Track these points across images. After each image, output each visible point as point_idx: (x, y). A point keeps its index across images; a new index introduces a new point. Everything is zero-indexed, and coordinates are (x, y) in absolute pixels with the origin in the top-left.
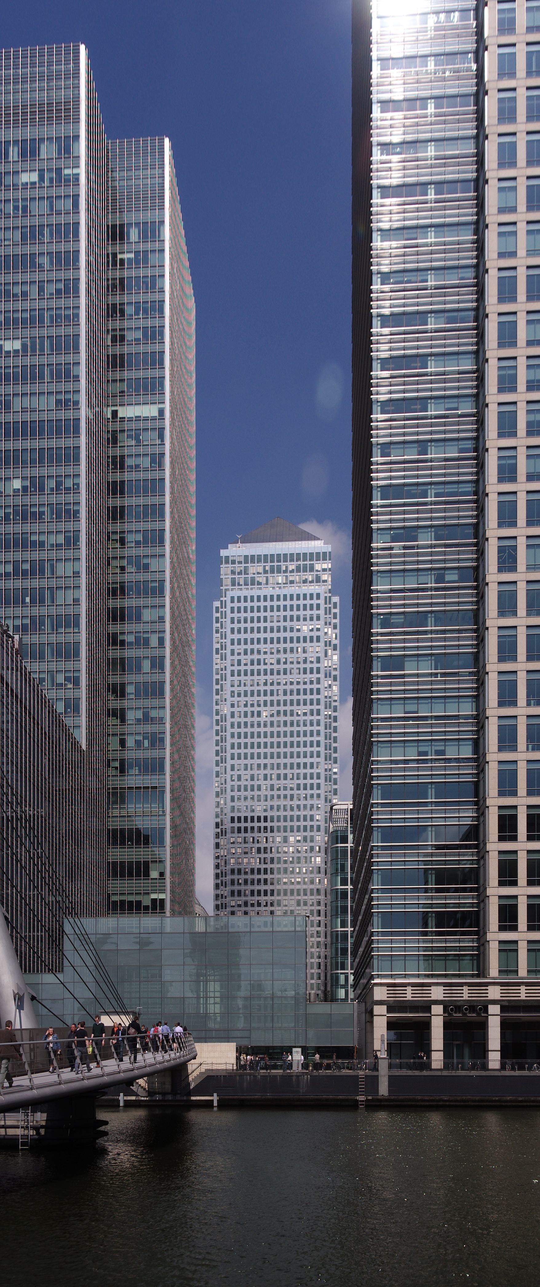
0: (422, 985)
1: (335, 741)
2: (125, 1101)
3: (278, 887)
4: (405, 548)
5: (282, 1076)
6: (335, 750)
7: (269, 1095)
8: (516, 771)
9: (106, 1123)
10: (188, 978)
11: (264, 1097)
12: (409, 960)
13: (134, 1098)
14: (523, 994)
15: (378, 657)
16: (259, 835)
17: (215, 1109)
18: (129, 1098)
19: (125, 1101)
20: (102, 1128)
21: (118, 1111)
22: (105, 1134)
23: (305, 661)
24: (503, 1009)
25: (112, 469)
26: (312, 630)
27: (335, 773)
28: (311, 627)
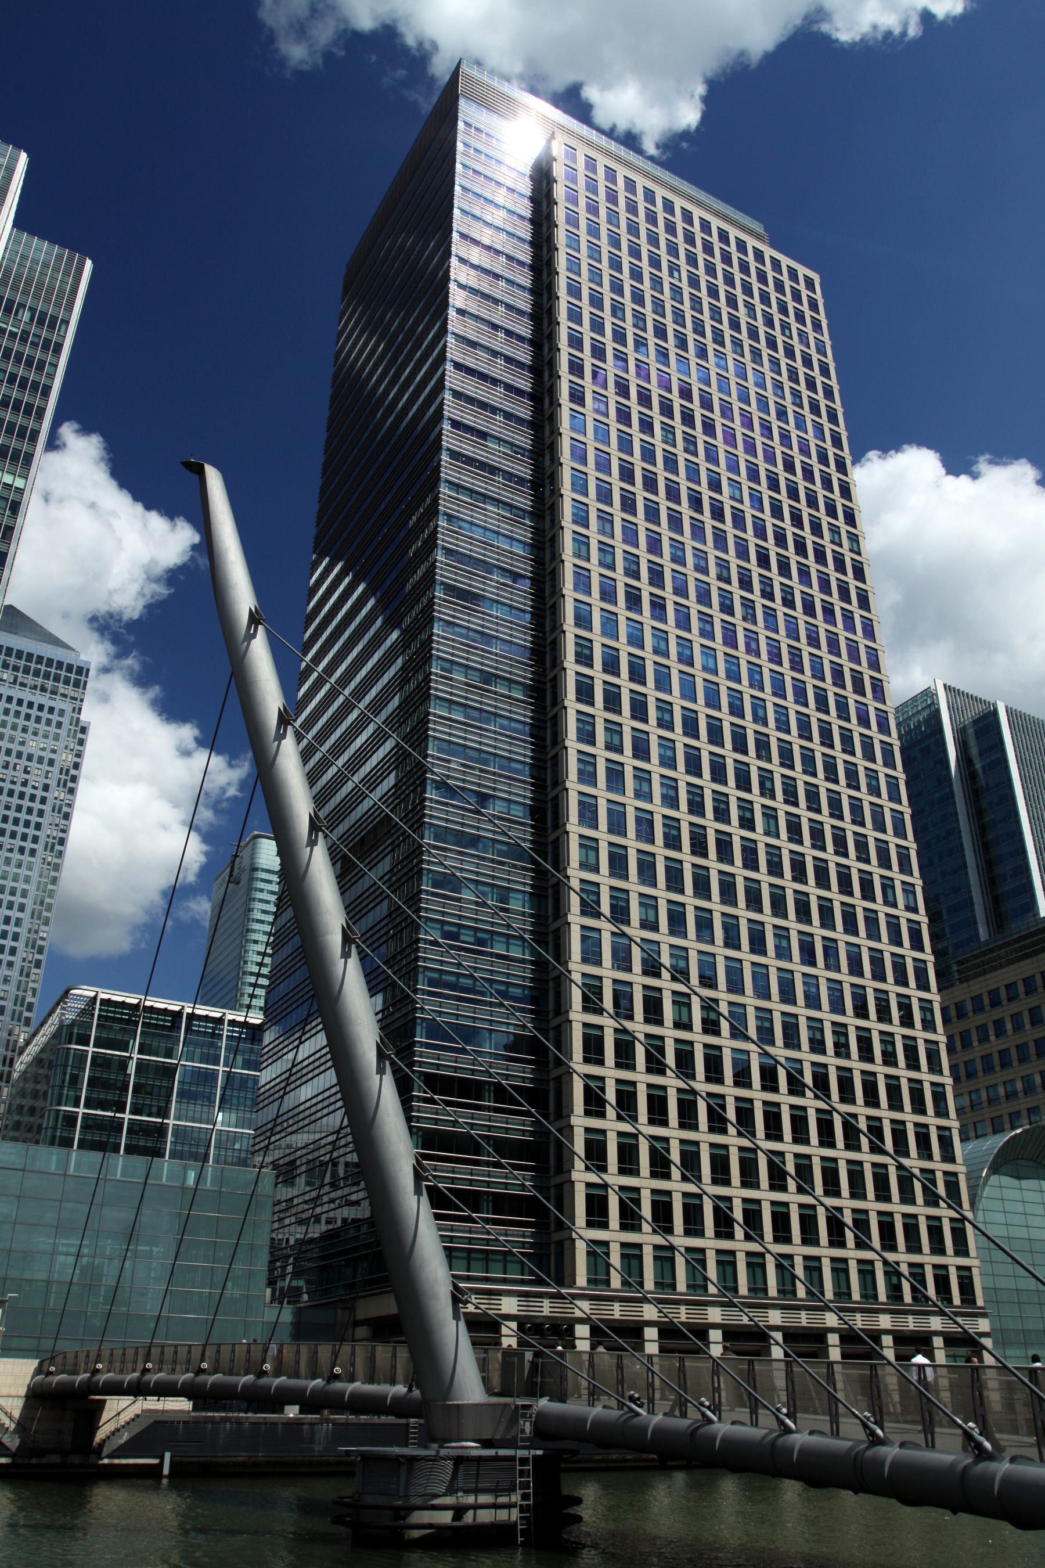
0: (490, 1292)
1: (51, 897)
4: (463, 765)
6: (49, 908)
7: (261, 1455)
10: (97, 1261)
11: (253, 1459)
12: (457, 1258)
20: (571, 1511)
23: (25, 784)
26: (44, 749)
27: (42, 939)
28: (42, 746)
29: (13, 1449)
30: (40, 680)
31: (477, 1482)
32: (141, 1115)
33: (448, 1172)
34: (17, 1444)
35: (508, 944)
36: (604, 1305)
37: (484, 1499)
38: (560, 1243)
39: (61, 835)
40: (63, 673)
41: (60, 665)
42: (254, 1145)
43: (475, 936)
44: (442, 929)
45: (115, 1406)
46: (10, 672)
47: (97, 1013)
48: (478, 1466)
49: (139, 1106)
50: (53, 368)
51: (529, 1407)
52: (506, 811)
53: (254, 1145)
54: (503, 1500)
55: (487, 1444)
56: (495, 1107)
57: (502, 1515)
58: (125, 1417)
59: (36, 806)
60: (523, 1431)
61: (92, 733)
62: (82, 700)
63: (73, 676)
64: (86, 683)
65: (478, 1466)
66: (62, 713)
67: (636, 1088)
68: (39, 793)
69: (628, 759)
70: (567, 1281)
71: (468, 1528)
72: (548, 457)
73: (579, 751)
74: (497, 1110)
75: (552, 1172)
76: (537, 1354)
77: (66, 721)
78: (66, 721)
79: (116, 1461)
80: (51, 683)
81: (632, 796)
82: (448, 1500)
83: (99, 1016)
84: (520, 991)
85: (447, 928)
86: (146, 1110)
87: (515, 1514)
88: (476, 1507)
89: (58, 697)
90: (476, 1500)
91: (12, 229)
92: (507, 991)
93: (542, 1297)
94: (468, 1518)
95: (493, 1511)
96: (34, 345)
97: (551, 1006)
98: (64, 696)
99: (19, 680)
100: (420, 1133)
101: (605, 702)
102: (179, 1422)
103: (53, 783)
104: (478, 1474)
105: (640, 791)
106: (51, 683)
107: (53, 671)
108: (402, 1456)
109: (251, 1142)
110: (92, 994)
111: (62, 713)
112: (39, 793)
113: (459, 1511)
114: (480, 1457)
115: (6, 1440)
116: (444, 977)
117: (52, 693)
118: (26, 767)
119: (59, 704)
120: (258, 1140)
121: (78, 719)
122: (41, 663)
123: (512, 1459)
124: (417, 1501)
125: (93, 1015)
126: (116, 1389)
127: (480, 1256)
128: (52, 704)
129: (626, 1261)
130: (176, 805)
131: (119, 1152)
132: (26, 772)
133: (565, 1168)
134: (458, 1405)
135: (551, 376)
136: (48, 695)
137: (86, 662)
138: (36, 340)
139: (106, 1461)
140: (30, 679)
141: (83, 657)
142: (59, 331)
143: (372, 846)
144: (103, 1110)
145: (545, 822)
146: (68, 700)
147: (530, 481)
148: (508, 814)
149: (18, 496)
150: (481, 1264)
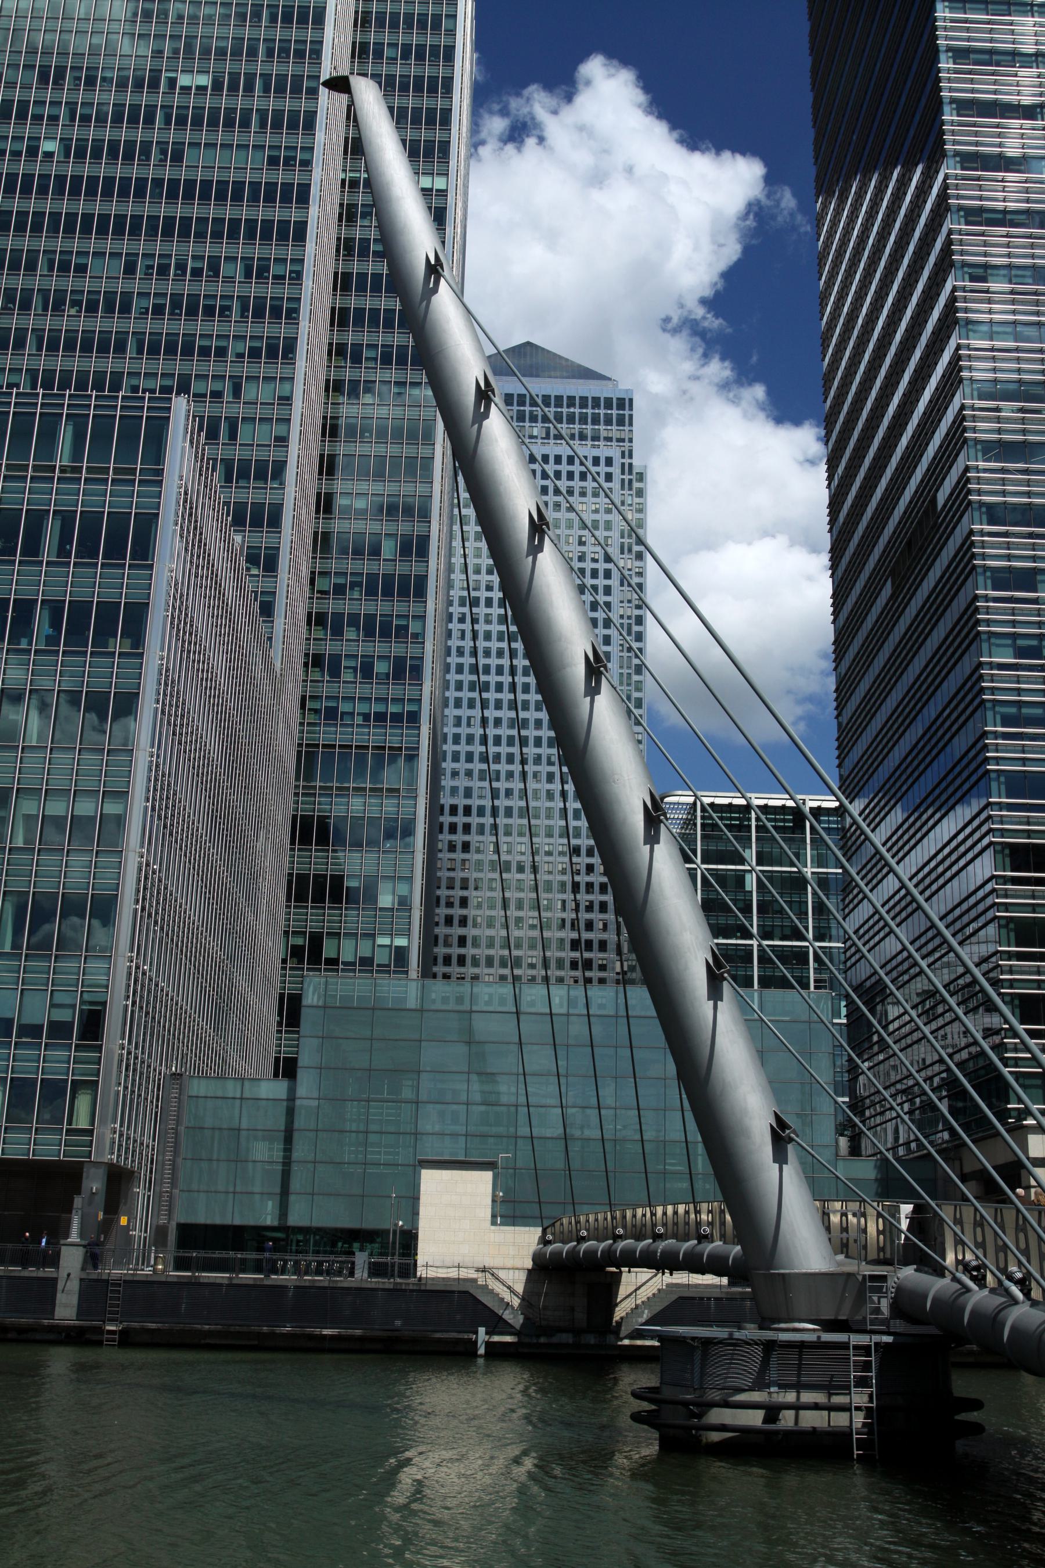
1: (638, 689)
2: (488, 1344)
3: (475, 932)
4: (1021, 410)
5: (296, 1287)
9: (976, 1405)
13: (508, 1339)
15: (986, 568)
16: (481, 838)
17: (481, 1361)
18: (496, 1338)
19: (488, 1344)
22: (977, 1428)
25: (344, 255)
26: (596, 511)
29: (518, 1326)
30: (577, 426)
31: (799, 1375)
32: (772, 939)
33: (1030, 974)
34: (521, 1321)
39: (637, 612)
40: (602, 412)
41: (596, 402)
42: (845, 962)
44: (1014, 646)
45: (634, 1280)
47: (699, 821)
48: (800, 1354)
50: (451, 21)
51: (883, 1278)
53: (845, 962)
54: (837, 1400)
55: (831, 1326)
57: (840, 1420)
58: (644, 1294)
59: (601, 582)
60: (877, 1310)
61: (649, 477)
62: (631, 440)
64: (631, 416)
65: (800, 1354)
66: (609, 462)
68: (602, 566)
71: (788, 1434)
77: (615, 470)
78: (615, 470)
79: (639, 1342)
80: (589, 427)
82: (756, 1396)
83: (702, 825)
86: (777, 932)
87: (859, 1419)
88: (797, 1407)
89: (602, 443)
90: (798, 1398)
94: (787, 1418)
98: (609, 439)
99: (553, 432)
100: (1012, 926)
102: (709, 1299)
103: (614, 551)
104: (800, 1365)
106: (589, 427)
107: (590, 411)
110: (691, 800)
111: (609, 462)
112: (602, 566)
113: (772, 1412)
114: (803, 1342)
115: (507, 1316)
116: (1024, 711)
117: (594, 439)
118: (580, 537)
119: (604, 451)
120: (848, 954)
121: (630, 465)
122: (574, 405)
123: (845, 1346)
124: (715, 1396)
125: (695, 825)
126: (632, 1261)
130: (814, 550)
131: (753, 987)
132: (581, 543)
134: (783, 1275)
136: (589, 443)
137: (627, 391)
139: (626, 1342)
140: (564, 428)
141: (622, 386)
143: (920, 549)
146: (615, 443)
149: (441, 199)
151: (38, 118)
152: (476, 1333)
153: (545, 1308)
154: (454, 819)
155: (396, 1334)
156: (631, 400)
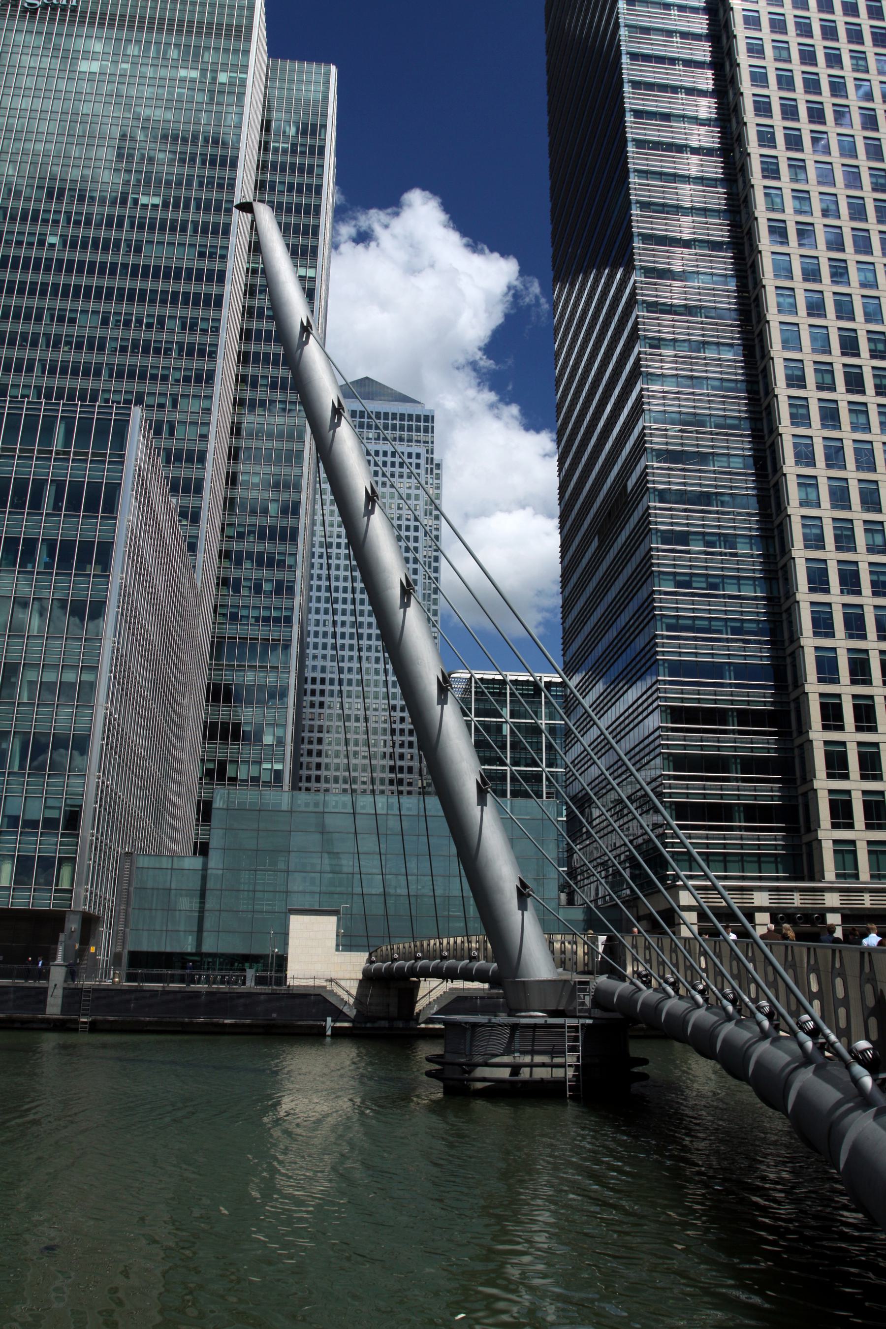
0: (742, 889)
2: (333, 1028)
3: (326, 760)
8: (868, 660)
9: (645, 1062)
13: (346, 1025)
14: (867, 901)
17: (328, 1039)
18: (338, 1024)
19: (333, 1028)
21: (323, 1044)
22: (644, 1077)
24: (845, 918)
26: (410, 488)
30: (398, 433)
31: (533, 1045)
35: (739, 585)
36: (854, 896)
37: (538, 1059)
38: (809, 844)
41: (410, 417)
43: (707, 582)
46: (373, 431)
47: (473, 690)
48: (534, 1032)
49: (517, 760)
51: (587, 983)
52: (726, 465)
54: (557, 1060)
56: (739, 730)
57: (559, 1073)
58: (435, 995)
59: (412, 534)
60: (583, 1003)
62: (432, 442)
63: (422, 424)
64: (433, 427)
65: (534, 1032)
66: (418, 456)
67: (873, 701)
69: (842, 396)
70: (817, 876)
71: (525, 1082)
72: (734, 121)
73: (849, 403)
74: (741, 732)
75: (799, 782)
76: (610, 939)
77: (422, 461)
78: (422, 461)
79: (431, 1026)
80: (406, 433)
81: (849, 429)
82: (506, 1059)
84: (755, 625)
85: (679, 578)
87: (570, 1072)
88: (531, 1066)
89: (414, 444)
90: (532, 1060)
91: (269, 60)
92: (742, 628)
93: (792, 891)
95: (549, 1069)
96: (303, 153)
97: (786, 635)
98: (418, 441)
99: (382, 436)
100: (671, 758)
101: (841, 348)
102: (476, 997)
103: (420, 514)
104: (534, 1038)
105: (857, 423)
107: (406, 423)
108: (466, 1023)
109: (564, 778)
110: (468, 676)
111: (418, 456)
112: (412, 523)
113: (516, 1069)
114: (535, 1024)
115: (346, 1010)
116: (680, 621)
117: (409, 441)
118: (399, 504)
119: (415, 449)
121: (432, 458)
122: (396, 419)
123: (562, 1026)
124: (479, 1059)
125: (471, 692)
126: (427, 973)
127: (736, 859)
128: (409, 450)
129: (874, 857)
130: (550, 516)
133: (808, 778)
135: (728, 38)
136: (406, 443)
138: (303, 149)
139: (423, 1026)
140: (389, 434)
142: (320, 135)
144: (489, 765)
145: (766, 469)
146: (422, 444)
147: (719, 149)
148: (729, 467)
150: (737, 865)
151: (45, 221)
152: (325, 1021)
153: (370, 1004)
154: (314, 687)
155: (273, 1022)
156: (433, 417)
